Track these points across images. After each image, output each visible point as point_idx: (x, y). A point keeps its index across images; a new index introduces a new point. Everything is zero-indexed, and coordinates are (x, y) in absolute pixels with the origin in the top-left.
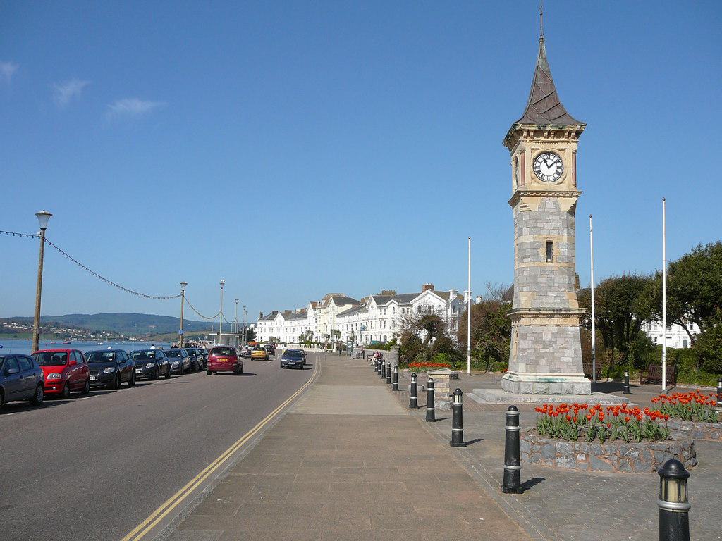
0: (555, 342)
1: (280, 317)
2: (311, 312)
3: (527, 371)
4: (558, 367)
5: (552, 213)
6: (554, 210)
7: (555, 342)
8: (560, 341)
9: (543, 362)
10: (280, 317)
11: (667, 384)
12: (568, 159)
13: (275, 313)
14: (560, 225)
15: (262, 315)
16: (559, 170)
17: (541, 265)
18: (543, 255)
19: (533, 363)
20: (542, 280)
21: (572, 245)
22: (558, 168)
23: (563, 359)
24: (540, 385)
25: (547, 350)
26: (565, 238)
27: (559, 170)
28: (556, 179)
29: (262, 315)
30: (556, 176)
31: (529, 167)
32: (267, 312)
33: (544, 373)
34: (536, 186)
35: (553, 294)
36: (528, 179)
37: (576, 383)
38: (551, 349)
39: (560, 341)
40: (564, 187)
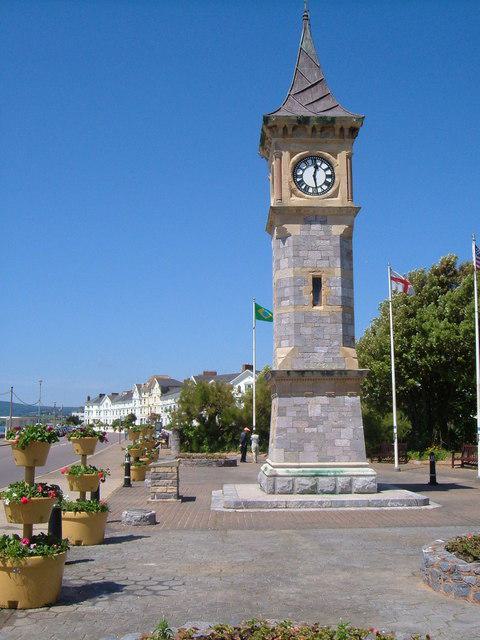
0: (326, 418)
1: (107, 401)
2: (136, 396)
3: (286, 460)
4: (329, 453)
5: (320, 238)
6: (338, 230)
7: (326, 418)
8: (333, 416)
9: (309, 447)
10: (107, 401)
11: (400, 462)
12: (340, 162)
13: (102, 396)
14: (331, 253)
15: (89, 398)
16: (329, 180)
17: (306, 309)
18: (309, 297)
19: (294, 449)
20: (307, 331)
21: (348, 282)
22: (327, 176)
23: (338, 442)
24: (304, 481)
25: (315, 430)
26: (338, 272)
27: (329, 180)
28: (324, 192)
29: (89, 398)
30: (325, 187)
31: (287, 176)
32: (95, 396)
33: (311, 464)
34: (296, 201)
35: (323, 350)
36: (286, 193)
37: (357, 476)
38: (321, 429)
39: (333, 416)
40: (336, 202)
